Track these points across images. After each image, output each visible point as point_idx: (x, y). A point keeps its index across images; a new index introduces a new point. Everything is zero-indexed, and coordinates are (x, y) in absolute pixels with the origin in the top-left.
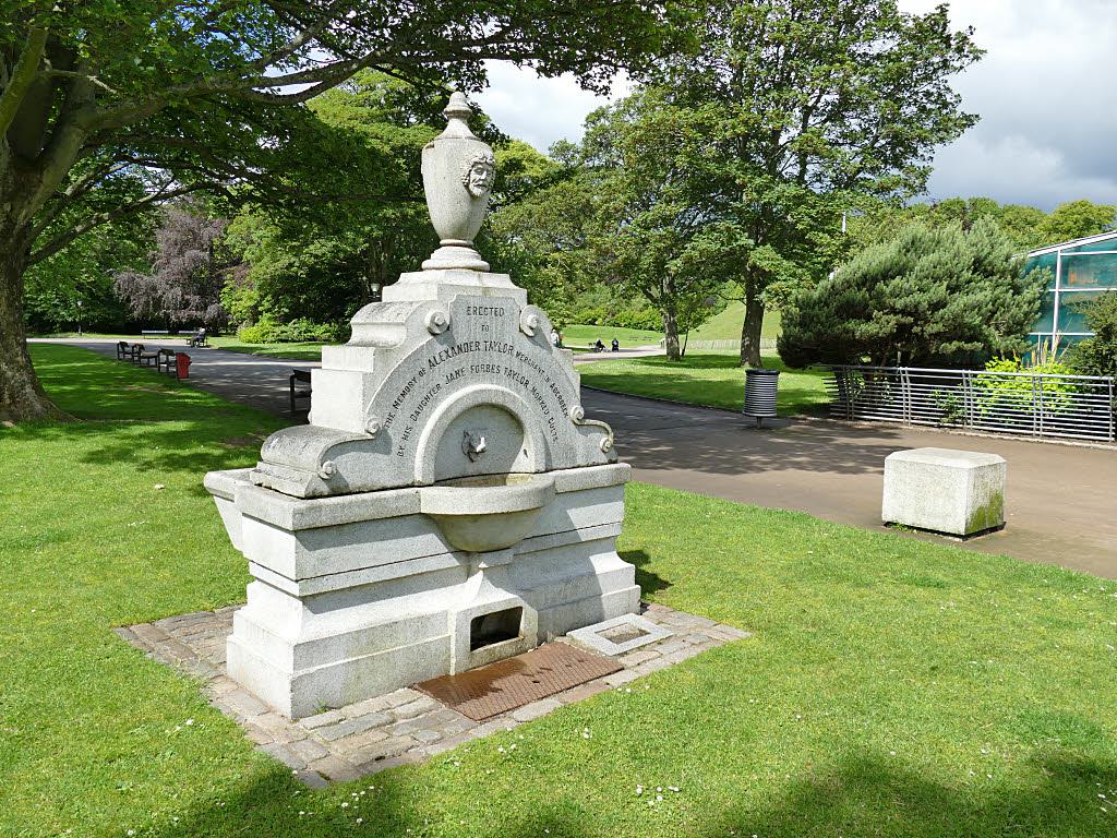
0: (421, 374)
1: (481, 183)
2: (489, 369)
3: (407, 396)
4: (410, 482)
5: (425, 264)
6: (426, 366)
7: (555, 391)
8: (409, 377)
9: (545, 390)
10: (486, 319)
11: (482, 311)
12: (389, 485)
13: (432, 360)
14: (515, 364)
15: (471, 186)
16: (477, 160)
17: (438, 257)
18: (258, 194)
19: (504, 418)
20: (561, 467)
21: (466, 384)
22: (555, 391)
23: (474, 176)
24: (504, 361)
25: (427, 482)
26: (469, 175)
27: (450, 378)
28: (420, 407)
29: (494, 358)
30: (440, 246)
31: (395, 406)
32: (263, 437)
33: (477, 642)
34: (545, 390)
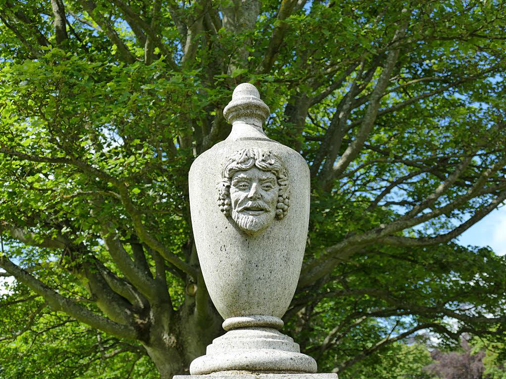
15: (234, 214)
16: (234, 165)
23: (236, 195)
26: (228, 195)
30: (222, 332)
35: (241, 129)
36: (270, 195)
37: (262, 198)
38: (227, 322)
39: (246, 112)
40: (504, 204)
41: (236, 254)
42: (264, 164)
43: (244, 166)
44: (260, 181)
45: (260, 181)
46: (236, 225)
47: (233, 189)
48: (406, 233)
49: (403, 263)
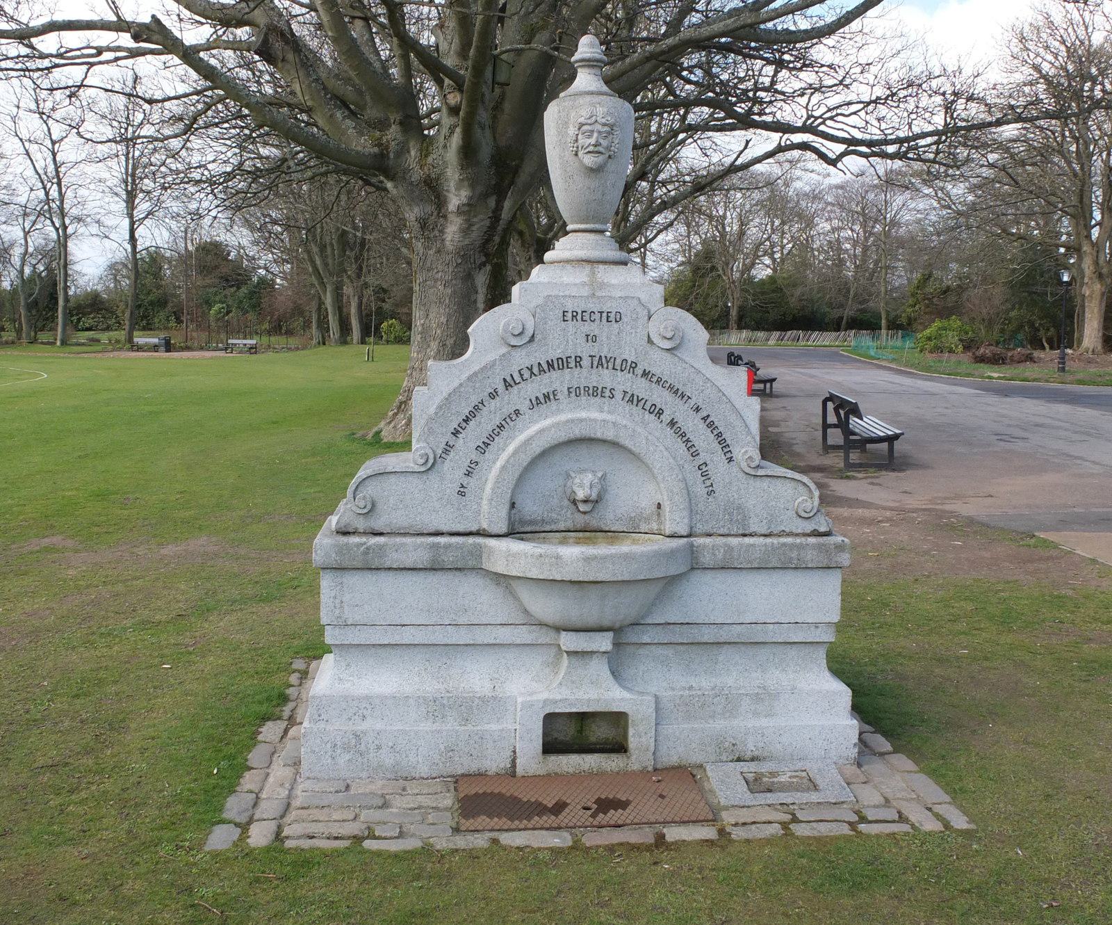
0: (493, 395)
1: (591, 148)
2: (596, 392)
3: (472, 423)
4: (474, 528)
5: (548, 256)
6: (501, 388)
7: (711, 425)
8: (474, 400)
9: (692, 425)
10: (593, 328)
11: (587, 317)
12: (445, 528)
13: (509, 379)
14: (641, 387)
15: (580, 154)
16: (582, 120)
17: (562, 249)
18: (682, 112)
19: (583, 450)
20: (722, 531)
21: (559, 411)
22: (711, 425)
23: (583, 141)
24: (623, 382)
25: (495, 530)
26: (577, 141)
27: (536, 403)
28: (491, 437)
29: (605, 378)
30: (567, 233)
31: (456, 433)
32: (347, 481)
33: (551, 747)
34: (692, 425)
35: (585, 80)
36: (604, 143)
37: (600, 145)
38: (569, 228)
39: (589, 63)
40: (371, 357)
41: (581, 182)
42: (604, 121)
43: (589, 121)
44: (599, 132)
45: (599, 132)
46: (581, 162)
47: (580, 137)
48: (762, 26)
49: (668, 510)
